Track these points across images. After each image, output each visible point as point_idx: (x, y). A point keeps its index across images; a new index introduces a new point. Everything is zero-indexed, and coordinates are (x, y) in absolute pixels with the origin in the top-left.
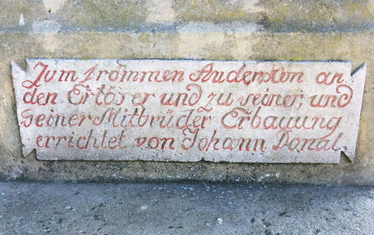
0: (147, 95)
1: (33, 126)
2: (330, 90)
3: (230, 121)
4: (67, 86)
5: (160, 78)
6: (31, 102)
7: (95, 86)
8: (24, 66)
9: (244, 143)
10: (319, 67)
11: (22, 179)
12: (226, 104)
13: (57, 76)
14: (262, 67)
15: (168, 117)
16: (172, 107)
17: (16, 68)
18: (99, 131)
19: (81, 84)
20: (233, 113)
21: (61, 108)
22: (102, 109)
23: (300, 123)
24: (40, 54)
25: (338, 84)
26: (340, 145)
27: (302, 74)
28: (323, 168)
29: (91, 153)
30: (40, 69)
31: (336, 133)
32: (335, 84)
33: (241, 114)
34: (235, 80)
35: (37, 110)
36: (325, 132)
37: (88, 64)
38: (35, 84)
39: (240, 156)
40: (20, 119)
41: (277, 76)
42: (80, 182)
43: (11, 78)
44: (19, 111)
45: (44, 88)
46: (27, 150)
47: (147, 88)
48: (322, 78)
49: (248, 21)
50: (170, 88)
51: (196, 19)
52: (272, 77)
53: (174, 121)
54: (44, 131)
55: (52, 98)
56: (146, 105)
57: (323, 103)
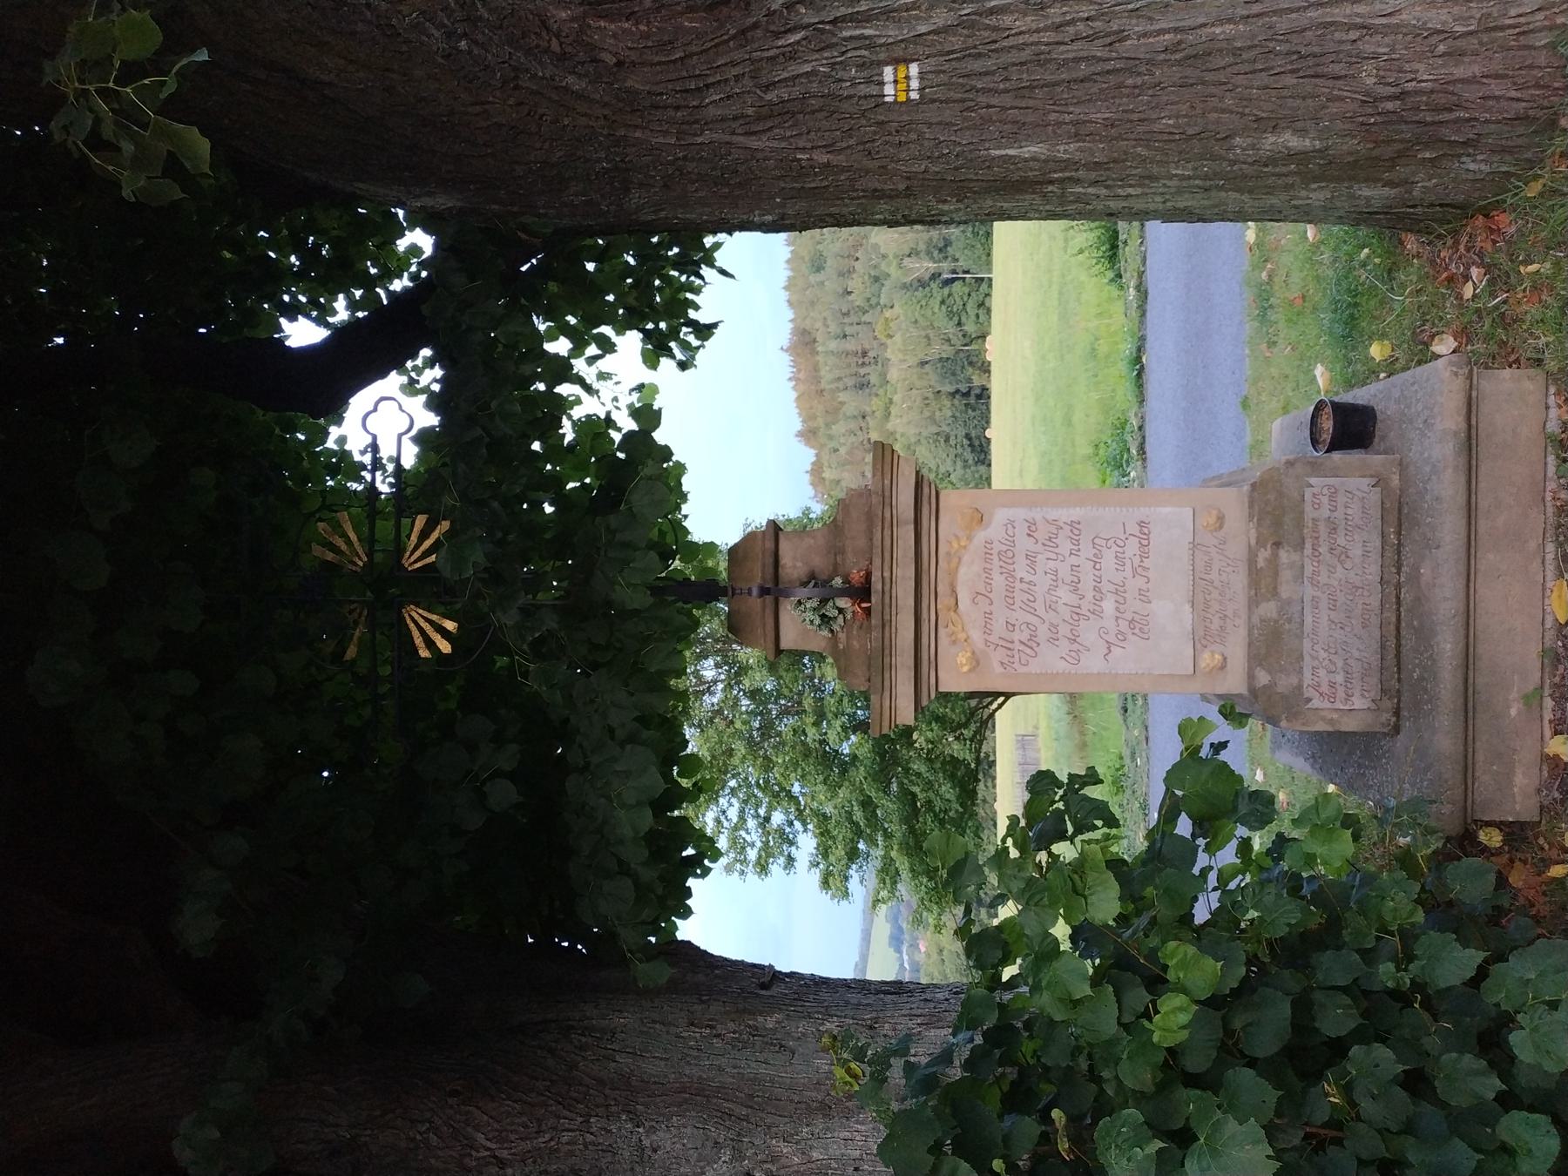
0: (1330, 620)
1: (1353, 699)
2: (1325, 500)
3: (1348, 565)
4: (1322, 673)
5: (1317, 611)
6: (1334, 698)
7: (1323, 654)
8: (1309, 700)
9: (1366, 554)
10: (1308, 508)
11: (1397, 713)
12: (1334, 568)
13: (1316, 679)
14: (1308, 546)
15: (1345, 607)
16: (1338, 604)
17: (1309, 706)
18: (1356, 654)
19: (1321, 663)
20: (1341, 563)
21: (1340, 678)
22: (1340, 651)
23: (1350, 518)
24: (1300, 687)
25: (1000, 1137)
26: (1366, 489)
27: (1313, 519)
28: (896, 398)
29: (1375, 660)
30: (1310, 688)
31: (1357, 493)
32: (1320, 497)
33: (1343, 557)
34: (1318, 562)
35: (1341, 694)
36: (1356, 499)
37: (1307, 658)
38: (1321, 694)
39: (1375, 556)
40: (1347, 707)
41: (1315, 535)
42: (1399, 672)
43: (1317, 709)
44: (1342, 707)
45: (1325, 688)
46: (1373, 706)
47: (1324, 620)
48: (1316, 506)
49: (1277, 555)
50: (1324, 604)
51: (1275, 588)
52: (1317, 538)
53: (1349, 602)
54: (1357, 693)
55: (1332, 685)
56: (1336, 621)
57: (1332, 503)
